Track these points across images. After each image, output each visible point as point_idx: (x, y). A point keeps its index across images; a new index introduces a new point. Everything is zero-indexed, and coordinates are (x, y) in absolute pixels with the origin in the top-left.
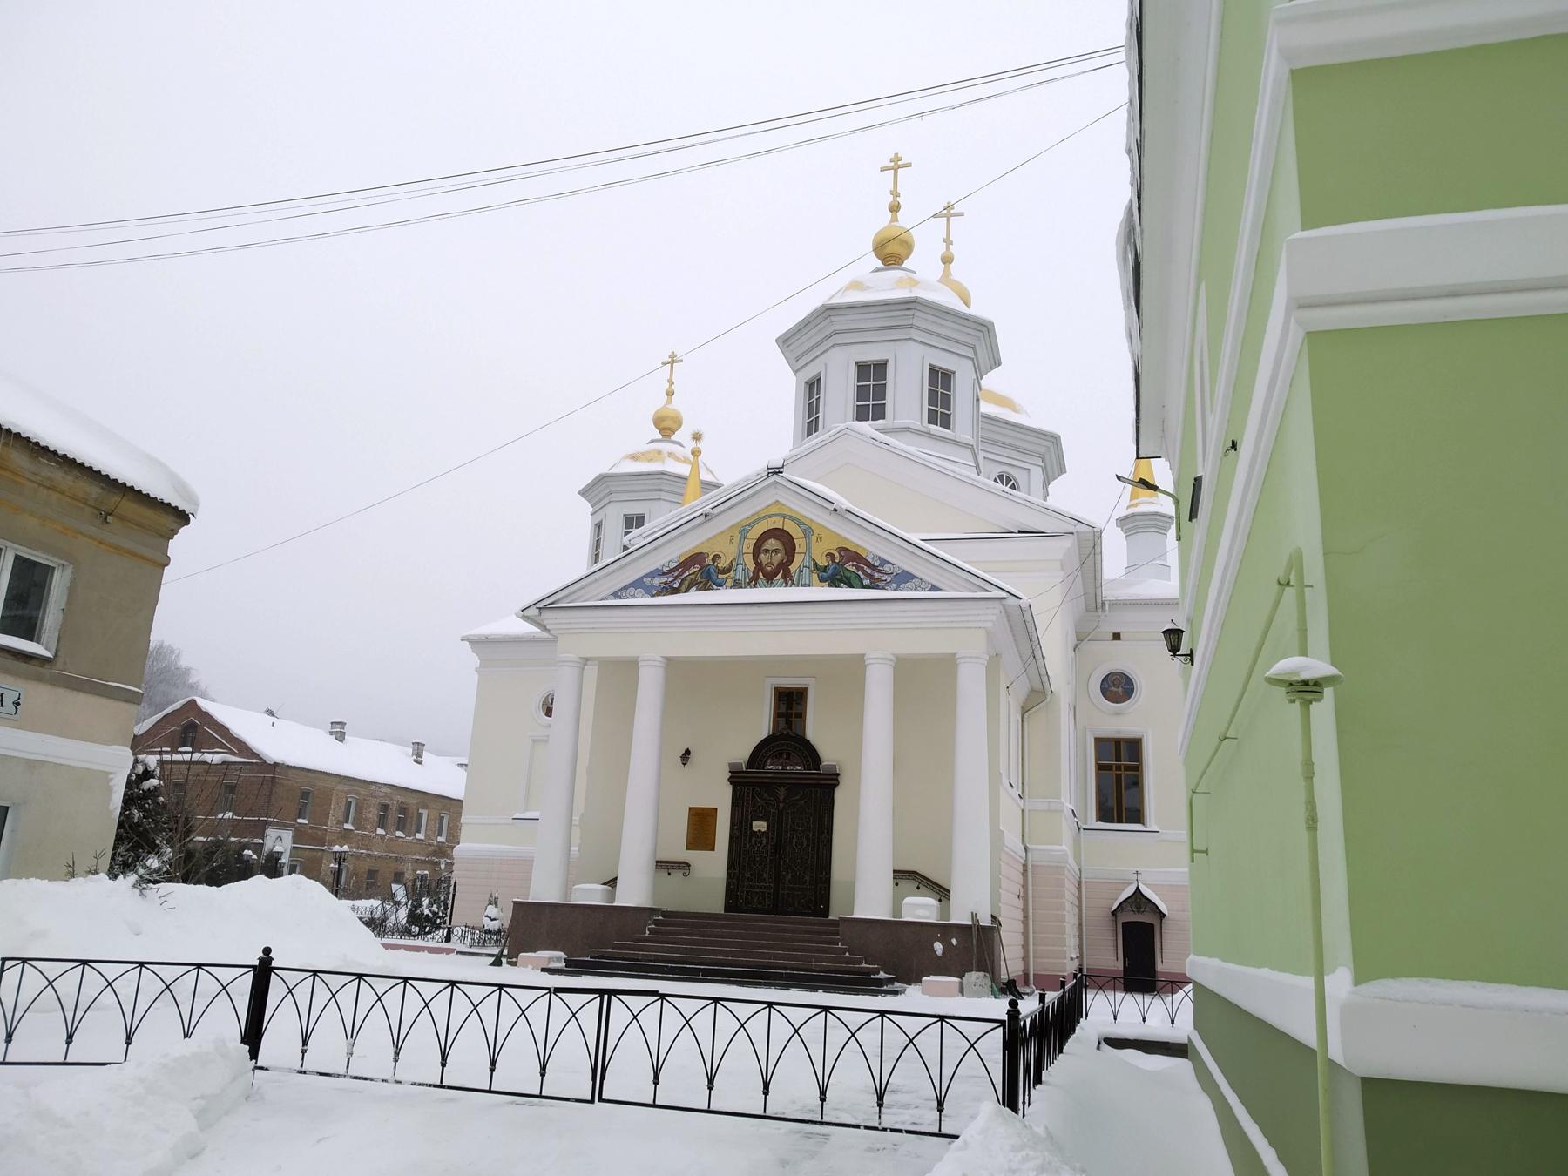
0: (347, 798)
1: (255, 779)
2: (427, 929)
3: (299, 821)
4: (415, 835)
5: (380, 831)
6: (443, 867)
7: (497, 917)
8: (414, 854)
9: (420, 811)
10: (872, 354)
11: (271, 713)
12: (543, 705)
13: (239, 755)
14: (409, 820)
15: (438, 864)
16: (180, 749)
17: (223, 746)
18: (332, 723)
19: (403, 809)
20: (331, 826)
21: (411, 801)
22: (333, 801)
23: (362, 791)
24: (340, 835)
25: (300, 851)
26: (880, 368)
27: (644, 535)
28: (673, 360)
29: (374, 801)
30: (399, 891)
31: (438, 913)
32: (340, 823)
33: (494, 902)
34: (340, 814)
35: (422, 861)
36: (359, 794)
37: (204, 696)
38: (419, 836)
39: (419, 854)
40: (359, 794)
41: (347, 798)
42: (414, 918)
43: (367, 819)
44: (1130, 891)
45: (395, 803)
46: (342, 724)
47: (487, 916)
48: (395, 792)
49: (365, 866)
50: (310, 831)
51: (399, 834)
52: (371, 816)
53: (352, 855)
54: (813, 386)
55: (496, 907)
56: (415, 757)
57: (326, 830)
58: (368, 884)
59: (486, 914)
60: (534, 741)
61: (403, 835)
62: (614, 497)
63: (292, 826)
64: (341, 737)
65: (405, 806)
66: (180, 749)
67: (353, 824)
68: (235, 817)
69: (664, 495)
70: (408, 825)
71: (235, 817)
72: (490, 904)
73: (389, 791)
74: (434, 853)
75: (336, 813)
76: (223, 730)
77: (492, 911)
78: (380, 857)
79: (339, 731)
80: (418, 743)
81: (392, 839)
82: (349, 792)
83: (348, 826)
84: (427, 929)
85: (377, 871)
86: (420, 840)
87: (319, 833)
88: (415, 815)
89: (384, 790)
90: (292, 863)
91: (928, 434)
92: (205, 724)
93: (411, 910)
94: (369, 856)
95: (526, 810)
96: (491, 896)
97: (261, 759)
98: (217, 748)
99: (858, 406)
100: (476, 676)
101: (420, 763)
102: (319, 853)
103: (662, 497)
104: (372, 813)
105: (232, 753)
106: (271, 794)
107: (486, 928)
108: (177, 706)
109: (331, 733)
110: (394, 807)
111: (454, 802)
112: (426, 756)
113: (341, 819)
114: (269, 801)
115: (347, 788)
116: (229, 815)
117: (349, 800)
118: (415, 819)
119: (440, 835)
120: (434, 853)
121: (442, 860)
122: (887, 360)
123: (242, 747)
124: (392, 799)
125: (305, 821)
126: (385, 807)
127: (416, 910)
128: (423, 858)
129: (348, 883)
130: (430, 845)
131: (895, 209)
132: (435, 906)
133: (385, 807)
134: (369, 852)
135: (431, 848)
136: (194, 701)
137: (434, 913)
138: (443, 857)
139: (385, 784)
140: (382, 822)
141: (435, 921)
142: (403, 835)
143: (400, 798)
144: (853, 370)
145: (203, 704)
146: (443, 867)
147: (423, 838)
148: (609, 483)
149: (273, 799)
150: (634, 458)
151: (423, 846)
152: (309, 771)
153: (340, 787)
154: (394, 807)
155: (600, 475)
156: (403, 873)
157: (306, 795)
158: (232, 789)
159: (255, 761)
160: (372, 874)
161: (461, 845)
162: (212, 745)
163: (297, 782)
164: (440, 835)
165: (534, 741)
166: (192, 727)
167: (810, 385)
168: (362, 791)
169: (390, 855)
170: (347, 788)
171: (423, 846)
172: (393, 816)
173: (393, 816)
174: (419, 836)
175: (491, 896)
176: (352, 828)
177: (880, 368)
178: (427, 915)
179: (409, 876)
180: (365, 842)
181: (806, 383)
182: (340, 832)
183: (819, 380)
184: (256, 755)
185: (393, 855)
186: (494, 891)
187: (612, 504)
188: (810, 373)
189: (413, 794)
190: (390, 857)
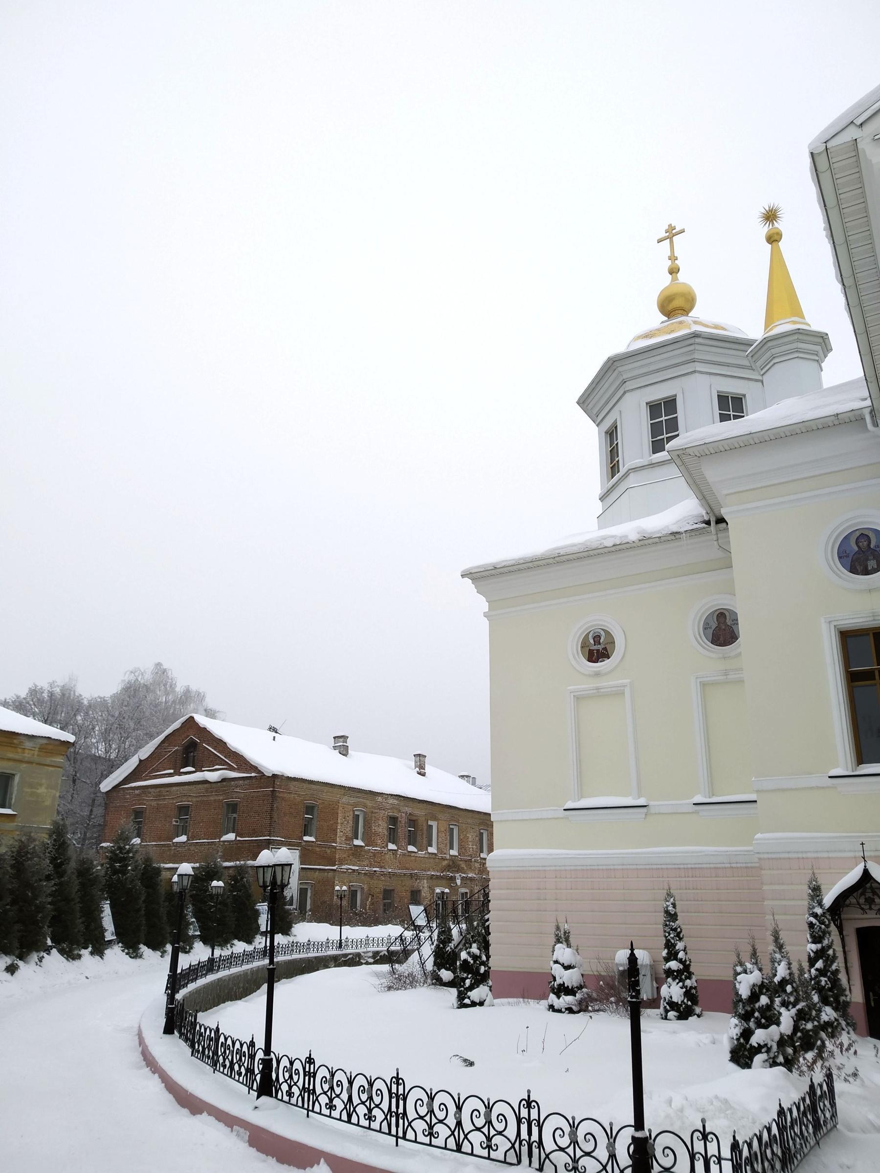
0: (354, 811)
1: (256, 794)
2: (468, 982)
3: (306, 838)
4: (427, 849)
5: (392, 846)
6: (459, 882)
7: (573, 963)
8: (429, 870)
9: (430, 823)
10: (659, 393)
11: (273, 730)
12: (582, 647)
13: (238, 770)
14: (419, 833)
15: (453, 879)
16: (182, 770)
17: (223, 763)
18: (335, 738)
19: (412, 822)
20: (339, 843)
21: (419, 812)
22: (340, 816)
23: (369, 803)
24: (351, 852)
25: (309, 873)
26: (670, 404)
27: (859, 122)
28: (671, 233)
29: (382, 814)
30: (417, 911)
31: (480, 957)
32: (349, 839)
33: (563, 938)
34: (348, 830)
35: (438, 877)
36: (365, 806)
37: (211, 714)
38: (432, 850)
39: (434, 870)
40: (365, 806)
41: (354, 811)
42: (443, 958)
43: (377, 834)
44: (853, 876)
45: (404, 815)
46: (344, 738)
47: (556, 962)
48: (402, 804)
49: (380, 885)
50: (318, 849)
51: (411, 848)
52: (380, 830)
53: (365, 874)
54: (612, 434)
55: (569, 946)
56: (417, 769)
57: (335, 847)
58: (385, 905)
59: (554, 959)
60: (578, 698)
61: (415, 850)
62: (629, 385)
63: (299, 845)
64: (344, 751)
65: (414, 818)
66: (182, 770)
67: (362, 840)
68: (238, 838)
69: (699, 367)
70: (419, 838)
71: (238, 838)
72: (558, 941)
73: (396, 802)
74: (449, 868)
75: (343, 828)
76: (220, 744)
77: (563, 953)
78: (394, 874)
79: (342, 745)
80: (419, 755)
81: (404, 855)
82: (356, 805)
83: (358, 842)
84: (468, 982)
85: (393, 890)
86: (433, 854)
87: (329, 851)
88: (425, 828)
89: (391, 801)
90: (302, 887)
91: (652, 465)
92: (204, 742)
93: (438, 946)
94: (383, 875)
95: (581, 796)
96: (558, 928)
97: (259, 772)
98: (217, 765)
99: (652, 441)
100: (486, 622)
101: (423, 775)
102: (331, 874)
103: (698, 369)
104: (381, 827)
105: (231, 769)
106: (272, 810)
107: (559, 981)
108: (177, 725)
109: (335, 748)
110: (403, 819)
111: (461, 813)
112: (428, 769)
113: (350, 835)
114: (271, 818)
115: (353, 800)
116: (231, 836)
117: (356, 813)
118: (425, 832)
119: (452, 848)
120: (449, 868)
121: (457, 875)
122: (676, 396)
123: (239, 761)
124: (400, 811)
125: (312, 839)
126: (393, 820)
127: (444, 947)
128: (438, 874)
129: (363, 905)
130: (443, 859)
131: (674, 271)
132: (474, 945)
133: (393, 820)
134: (383, 870)
135: (445, 863)
136: (192, 718)
137: (475, 957)
138: (458, 872)
139: (392, 795)
140: (393, 838)
141: (478, 969)
142: (415, 850)
143: (408, 810)
144: (645, 412)
145: (202, 720)
146: (459, 882)
147: (436, 852)
148: (620, 369)
149: (275, 816)
150: (647, 336)
151: (437, 860)
152: (311, 782)
153: (345, 799)
154: (403, 819)
155: (609, 359)
156: (420, 891)
157: (310, 809)
158: (233, 807)
159: (253, 775)
160: (388, 893)
161: (496, 852)
162: (211, 762)
163: (299, 795)
164: (452, 848)
165: (578, 698)
166: (192, 746)
167: (610, 434)
168: (369, 803)
169: (404, 871)
170: (353, 800)
171: (437, 860)
172: (403, 830)
173: (403, 830)
174: (432, 850)
175: (558, 928)
176: (362, 844)
177: (670, 404)
178: (465, 961)
179: (425, 893)
180: (377, 858)
181: (647, 404)
182: (351, 849)
183: (616, 427)
184: (254, 768)
185: (408, 872)
186: (561, 920)
187: (627, 395)
188: (607, 424)
189: (421, 805)
190: (405, 874)
